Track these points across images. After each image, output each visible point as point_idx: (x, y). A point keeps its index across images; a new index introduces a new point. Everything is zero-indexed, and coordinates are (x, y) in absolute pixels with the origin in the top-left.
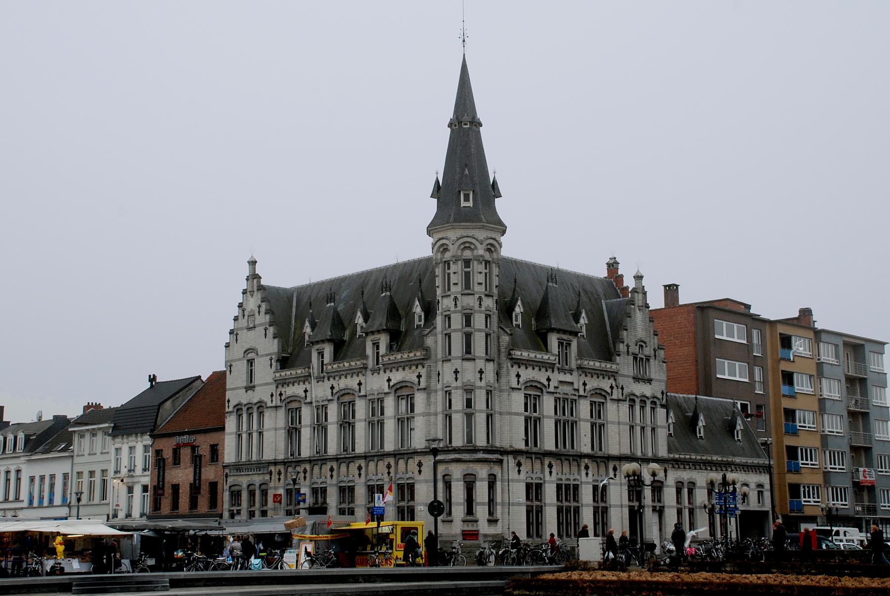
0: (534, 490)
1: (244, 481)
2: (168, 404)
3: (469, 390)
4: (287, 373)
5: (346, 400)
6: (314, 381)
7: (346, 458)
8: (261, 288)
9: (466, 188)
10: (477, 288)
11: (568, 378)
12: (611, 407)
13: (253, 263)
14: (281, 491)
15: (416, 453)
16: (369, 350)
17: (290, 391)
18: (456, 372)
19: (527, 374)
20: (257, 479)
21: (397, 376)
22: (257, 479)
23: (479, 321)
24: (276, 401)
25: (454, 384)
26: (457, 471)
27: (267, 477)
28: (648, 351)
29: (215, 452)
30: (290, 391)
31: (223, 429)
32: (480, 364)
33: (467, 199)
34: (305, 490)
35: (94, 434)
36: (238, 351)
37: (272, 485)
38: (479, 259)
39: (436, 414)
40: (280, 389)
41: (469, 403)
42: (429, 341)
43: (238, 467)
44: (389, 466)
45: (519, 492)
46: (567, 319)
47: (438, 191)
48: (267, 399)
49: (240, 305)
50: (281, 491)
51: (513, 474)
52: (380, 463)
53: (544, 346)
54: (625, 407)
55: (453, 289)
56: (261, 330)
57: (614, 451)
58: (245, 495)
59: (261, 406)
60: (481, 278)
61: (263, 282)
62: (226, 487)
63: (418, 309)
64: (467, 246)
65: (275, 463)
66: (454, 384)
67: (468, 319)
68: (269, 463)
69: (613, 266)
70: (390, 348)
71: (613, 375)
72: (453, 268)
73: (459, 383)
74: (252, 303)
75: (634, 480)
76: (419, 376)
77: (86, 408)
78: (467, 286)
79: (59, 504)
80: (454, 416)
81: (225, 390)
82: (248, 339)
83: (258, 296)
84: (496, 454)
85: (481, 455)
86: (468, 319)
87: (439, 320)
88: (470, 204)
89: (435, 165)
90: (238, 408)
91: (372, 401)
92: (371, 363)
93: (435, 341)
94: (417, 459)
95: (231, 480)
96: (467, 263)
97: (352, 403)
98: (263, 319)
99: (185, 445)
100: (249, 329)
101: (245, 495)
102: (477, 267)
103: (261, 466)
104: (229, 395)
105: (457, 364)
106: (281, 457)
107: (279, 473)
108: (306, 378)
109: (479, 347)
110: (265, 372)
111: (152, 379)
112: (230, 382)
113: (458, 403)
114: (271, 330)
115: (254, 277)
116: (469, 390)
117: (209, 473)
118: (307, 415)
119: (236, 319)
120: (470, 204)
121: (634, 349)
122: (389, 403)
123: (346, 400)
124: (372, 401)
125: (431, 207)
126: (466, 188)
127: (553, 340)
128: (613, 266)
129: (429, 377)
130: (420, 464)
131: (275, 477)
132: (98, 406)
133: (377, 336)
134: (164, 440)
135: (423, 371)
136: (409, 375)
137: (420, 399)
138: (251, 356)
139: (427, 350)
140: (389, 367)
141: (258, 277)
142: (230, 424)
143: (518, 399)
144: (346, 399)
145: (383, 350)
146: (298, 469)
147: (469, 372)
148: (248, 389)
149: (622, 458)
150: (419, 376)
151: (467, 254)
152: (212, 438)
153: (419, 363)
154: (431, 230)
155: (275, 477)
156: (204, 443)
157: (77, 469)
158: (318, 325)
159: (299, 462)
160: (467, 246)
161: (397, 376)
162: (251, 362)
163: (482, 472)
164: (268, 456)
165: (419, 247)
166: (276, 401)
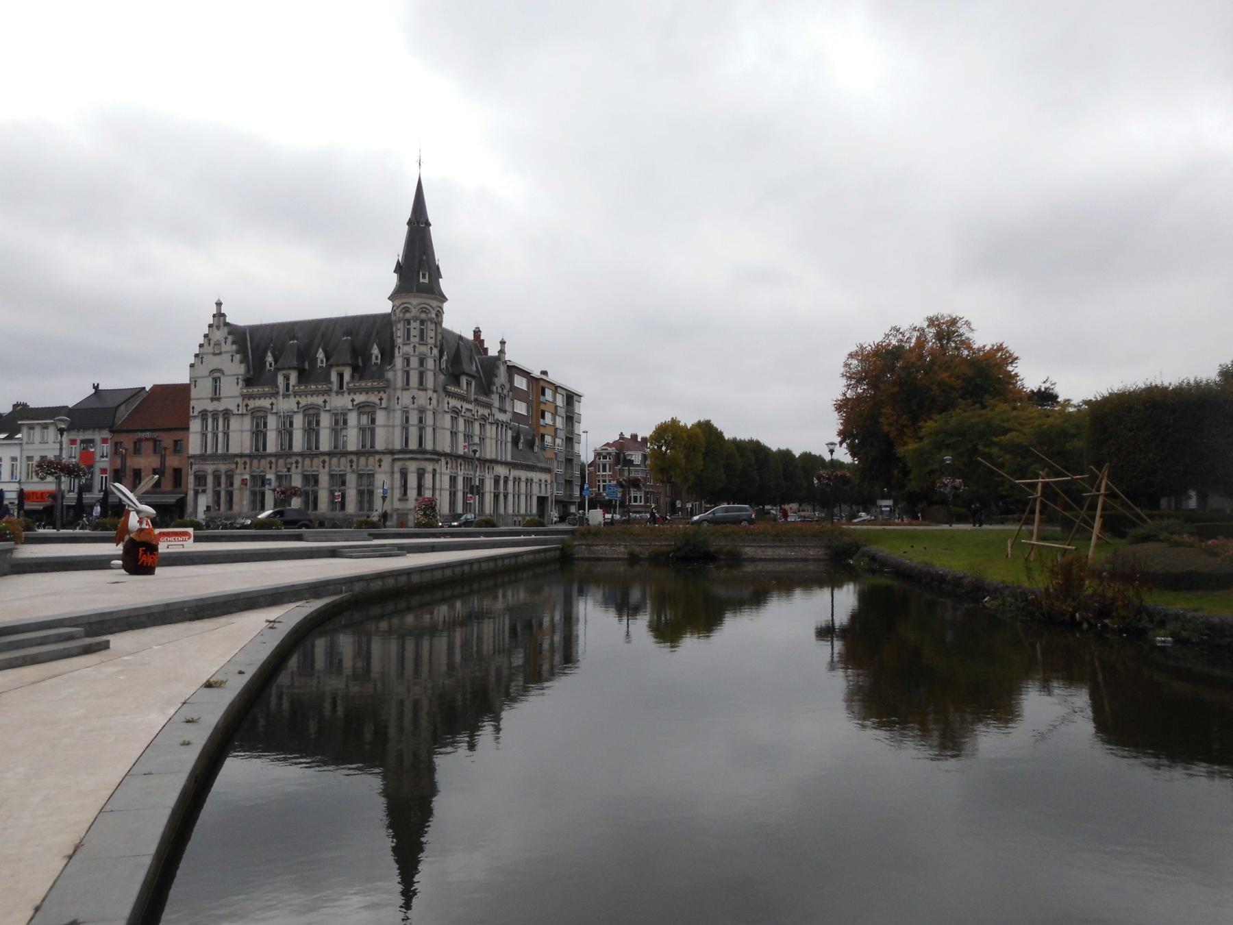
0: (453, 480)
1: (209, 468)
2: (122, 407)
3: (422, 411)
4: (255, 390)
5: (312, 415)
6: (281, 398)
7: (338, 452)
8: (227, 324)
9: (418, 267)
10: (430, 341)
11: (469, 406)
12: (488, 427)
13: (219, 304)
14: (247, 477)
15: (378, 453)
16: (280, 379)
17: (253, 404)
18: (413, 398)
19: (454, 403)
20: (223, 468)
21: (360, 398)
22: (223, 468)
23: (430, 364)
24: (242, 410)
25: (412, 406)
26: (412, 467)
27: (233, 466)
28: (505, 392)
29: (179, 447)
30: (253, 404)
31: (188, 429)
32: (430, 393)
33: (424, 277)
34: (270, 476)
35: (45, 427)
36: (203, 370)
37: (238, 471)
38: (431, 320)
39: (393, 426)
40: (246, 401)
41: (421, 420)
42: (390, 375)
43: (203, 457)
44: (351, 461)
45: (446, 479)
46: (472, 368)
47: (399, 269)
48: (233, 408)
49: (206, 336)
50: (247, 477)
51: (444, 470)
52: (371, 459)
53: (458, 384)
54: (494, 428)
55: (412, 339)
56: (228, 357)
57: (488, 457)
58: (210, 480)
59: (227, 414)
60: (432, 334)
61: (228, 320)
62: (191, 473)
63: (375, 351)
64: (424, 311)
65: (241, 456)
66: (412, 406)
67: (422, 362)
68: (236, 456)
69: (477, 333)
70: (352, 377)
71: (489, 406)
72: (413, 324)
73: (415, 406)
74: (219, 335)
75: (828, 485)
76: (381, 399)
77: (15, 406)
78: (422, 338)
79: (8, 479)
80: (377, 430)
81: (189, 399)
82: (213, 362)
83: (225, 330)
84: (436, 455)
85: (429, 456)
86: (422, 362)
87: (399, 362)
88: (426, 281)
89: (396, 248)
90: (204, 414)
91: (336, 415)
92: (335, 387)
93: (395, 374)
94: (377, 457)
95: (195, 467)
96: (422, 322)
97: (318, 415)
98: (229, 347)
99: (147, 439)
100: (215, 354)
101: (210, 480)
102: (414, 325)
103: (227, 457)
104: (192, 403)
105: (415, 392)
106: (247, 451)
107: (245, 463)
108: (275, 394)
109: (430, 381)
110: (231, 389)
111: (96, 387)
112: (194, 393)
113: (414, 419)
114: (238, 357)
115: (219, 315)
116: (422, 411)
117: (173, 461)
118: (272, 422)
119: (201, 346)
120: (426, 281)
121: (500, 390)
122: (352, 418)
123: (312, 415)
124: (336, 415)
125: (392, 281)
126: (418, 267)
127: (464, 380)
128: (477, 333)
129: (389, 400)
130: (380, 461)
131: (240, 466)
132: (25, 405)
133: (341, 368)
134: (124, 435)
135: (384, 396)
136: (374, 398)
137: (381, 417)
138: (216, 375)
139: (388, 381)
140: (350, 391)
141: (224, 315)
142: (195, 425)
143: (448, 418)
144: (311, 412)
145: (347, 378)
146: (289, 460)
147: (422, 398)
148: (212, 400)
149: (495, 462)
150: (381, 399)
151: (423, 316)
152: (177, 435)
153: (384, 389)
154: (391, 298)
155: (240, 466)
156: (167, 440)
157: (26, 454)
158: (273, 354)
159: (317, 455)
160: (424, 310)
161: (360, 398)
162: (216, 380)
163: (429, 467)
164: (234, 449)
165: (386, 307)
166: (242, 410)
